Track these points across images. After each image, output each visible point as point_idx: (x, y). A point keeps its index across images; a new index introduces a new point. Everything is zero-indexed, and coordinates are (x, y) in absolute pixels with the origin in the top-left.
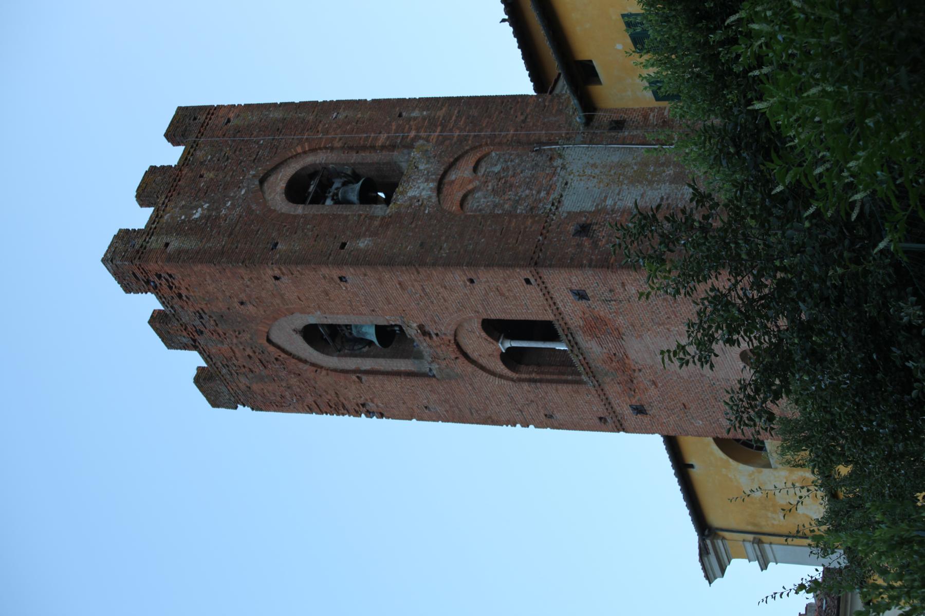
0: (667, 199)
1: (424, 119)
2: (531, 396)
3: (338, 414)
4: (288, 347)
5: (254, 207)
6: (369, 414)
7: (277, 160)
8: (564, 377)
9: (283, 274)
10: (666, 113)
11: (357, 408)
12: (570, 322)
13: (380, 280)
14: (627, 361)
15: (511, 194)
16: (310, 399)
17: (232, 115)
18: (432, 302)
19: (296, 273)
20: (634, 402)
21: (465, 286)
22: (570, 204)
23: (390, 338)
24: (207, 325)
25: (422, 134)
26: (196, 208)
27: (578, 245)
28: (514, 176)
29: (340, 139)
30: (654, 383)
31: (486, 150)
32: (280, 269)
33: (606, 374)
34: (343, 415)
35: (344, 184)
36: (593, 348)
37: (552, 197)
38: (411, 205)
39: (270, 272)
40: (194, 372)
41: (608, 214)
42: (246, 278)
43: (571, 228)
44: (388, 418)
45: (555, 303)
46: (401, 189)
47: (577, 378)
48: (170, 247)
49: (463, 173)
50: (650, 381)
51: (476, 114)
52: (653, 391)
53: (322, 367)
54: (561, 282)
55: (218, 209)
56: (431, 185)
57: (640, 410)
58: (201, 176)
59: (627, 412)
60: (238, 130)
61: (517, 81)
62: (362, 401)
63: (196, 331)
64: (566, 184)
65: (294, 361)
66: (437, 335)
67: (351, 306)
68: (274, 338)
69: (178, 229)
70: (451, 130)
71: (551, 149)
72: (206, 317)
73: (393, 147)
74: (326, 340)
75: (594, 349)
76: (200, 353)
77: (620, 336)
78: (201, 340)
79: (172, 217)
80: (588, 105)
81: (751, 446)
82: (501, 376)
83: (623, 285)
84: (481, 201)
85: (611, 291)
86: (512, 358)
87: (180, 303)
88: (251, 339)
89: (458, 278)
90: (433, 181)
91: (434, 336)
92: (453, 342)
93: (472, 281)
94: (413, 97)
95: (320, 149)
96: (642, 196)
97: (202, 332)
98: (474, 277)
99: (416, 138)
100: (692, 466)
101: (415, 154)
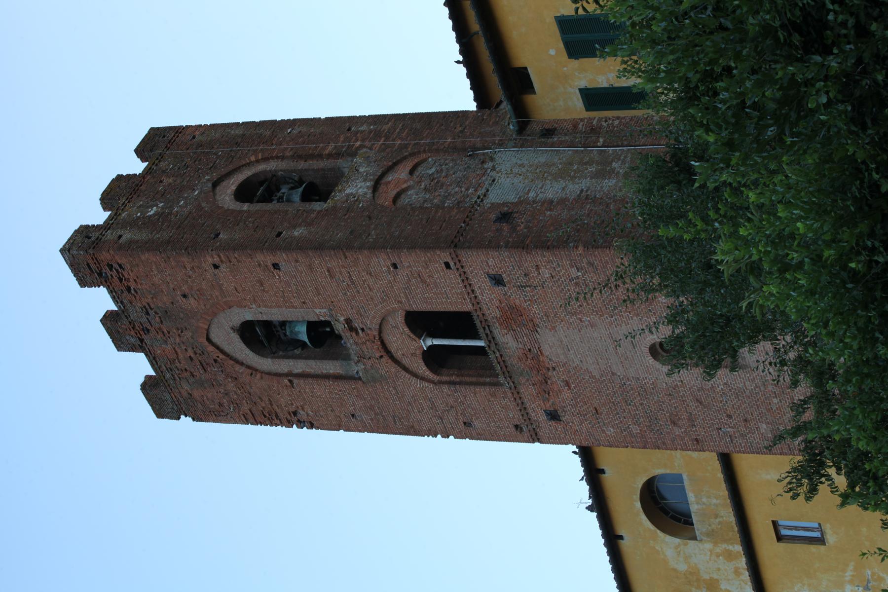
0: (587, 191)
1: (371, 132)
2: (451, 401)
3: (272, 425)
4: (226, 348)
5: (204, 205)
6: (301, 424)
7: (231, 167)
8: (482, 380)
9: (222, 261)
10: (595, 122)
11: (289, 417)
12: (487, 312)
13: (310, 267)
14: (541, 358)
15: (442, 192)
16: (245, 408)
17: (197, 133)
18: (358, 292)
19: (233, 260)
20: (548, 406)
21: (389, 272)
22: (494, 197)
23: (323, 337)
24: (153, 322)
25: (367, 143)
26: (152, 207)
27: (497, 230)
28: (446, 176)
29: (292, 149)
30: (567, 384)
31: (424, 156)
32: (219, 256)
33: (521, 374)
34: (276, 425)
35: (292, 188)
36: (510, 343)
37: (479, 193)
38: (347, 201)
39: (210, 260)
40: (142, 380)
41: (529, 204)
42: (188, 266)
43: (493, 216)
44: (317, 428)
45: (473, 291)
46: (340, 188)
47: (495, 379)
48: (123, 239)
49: (401, 174)
50: (563, 381)
51: (418, 127)
52: (566, 394)
53: (256, 370)
54: (479, 263)
55: (171, 207)
56: (368, 184)
57: (554, 416)
58: (161, 182)
59: (542, 417)
60: (200, 145)
61: (460, 97)
62: (292, 409)
63: (143, 329)
64: (494, 181)
65: (232, 362)
66: (363, 330)
67: (283, 297)
68: (215, 340)
69: (132, 224)
70: (394, 140)
71: (484, 154)
72: (152, 313)
73: (338, 155)
74: (261, 342)
75: (510, 344)
76: (147, 355)
77: (535, 329)
78: (147, 340)
79: (129, 215)
80: (522, 114)
81: (679, 520)
82: (423, 379)
83: (538, 268)
84: (413, 197)
85: (526, 275)
86: (435, 359)
87: (129, 297)
88: (192, 338)
89: (382, 263)
90: (371, 180)
91: (360, 331)
92: (377, 338)
93: (395, 266)
94: (362, 114)
95: (272, 158)
96: (563, 189)
97: (148, 330)
98: (397, 261)
99: (361, 147)
100: (621, 537)
101: (358, 160)
